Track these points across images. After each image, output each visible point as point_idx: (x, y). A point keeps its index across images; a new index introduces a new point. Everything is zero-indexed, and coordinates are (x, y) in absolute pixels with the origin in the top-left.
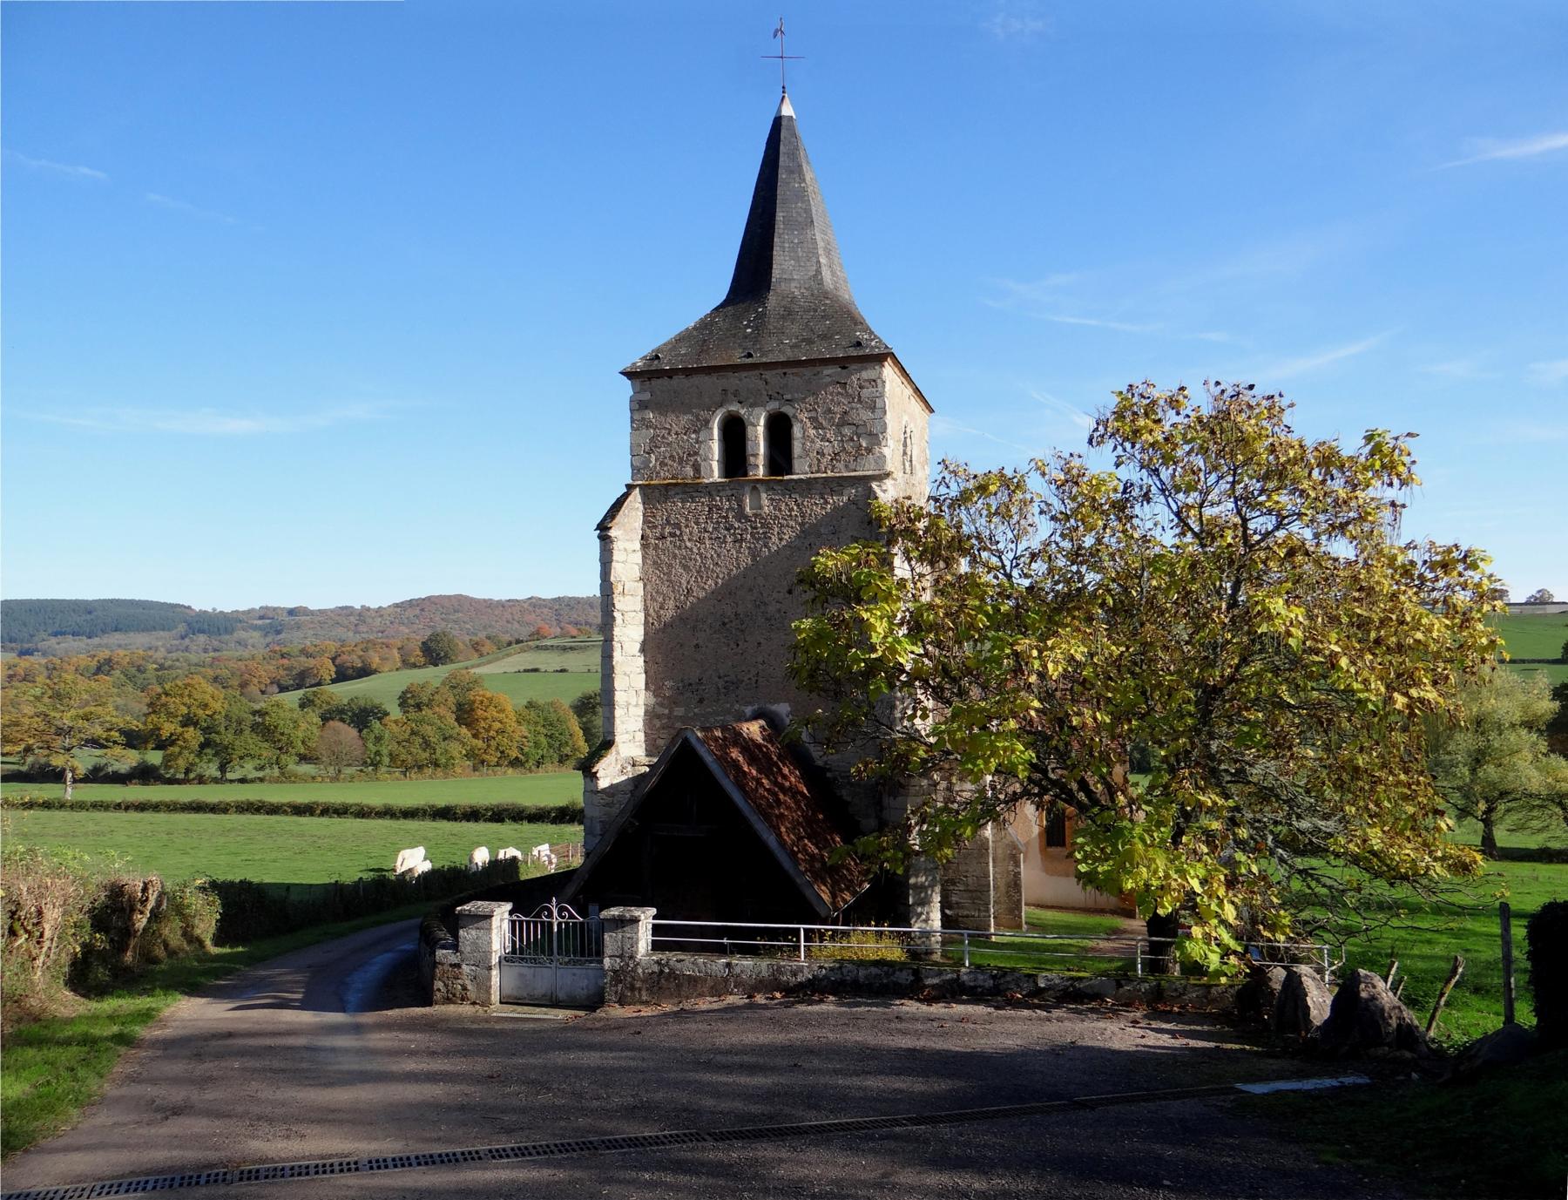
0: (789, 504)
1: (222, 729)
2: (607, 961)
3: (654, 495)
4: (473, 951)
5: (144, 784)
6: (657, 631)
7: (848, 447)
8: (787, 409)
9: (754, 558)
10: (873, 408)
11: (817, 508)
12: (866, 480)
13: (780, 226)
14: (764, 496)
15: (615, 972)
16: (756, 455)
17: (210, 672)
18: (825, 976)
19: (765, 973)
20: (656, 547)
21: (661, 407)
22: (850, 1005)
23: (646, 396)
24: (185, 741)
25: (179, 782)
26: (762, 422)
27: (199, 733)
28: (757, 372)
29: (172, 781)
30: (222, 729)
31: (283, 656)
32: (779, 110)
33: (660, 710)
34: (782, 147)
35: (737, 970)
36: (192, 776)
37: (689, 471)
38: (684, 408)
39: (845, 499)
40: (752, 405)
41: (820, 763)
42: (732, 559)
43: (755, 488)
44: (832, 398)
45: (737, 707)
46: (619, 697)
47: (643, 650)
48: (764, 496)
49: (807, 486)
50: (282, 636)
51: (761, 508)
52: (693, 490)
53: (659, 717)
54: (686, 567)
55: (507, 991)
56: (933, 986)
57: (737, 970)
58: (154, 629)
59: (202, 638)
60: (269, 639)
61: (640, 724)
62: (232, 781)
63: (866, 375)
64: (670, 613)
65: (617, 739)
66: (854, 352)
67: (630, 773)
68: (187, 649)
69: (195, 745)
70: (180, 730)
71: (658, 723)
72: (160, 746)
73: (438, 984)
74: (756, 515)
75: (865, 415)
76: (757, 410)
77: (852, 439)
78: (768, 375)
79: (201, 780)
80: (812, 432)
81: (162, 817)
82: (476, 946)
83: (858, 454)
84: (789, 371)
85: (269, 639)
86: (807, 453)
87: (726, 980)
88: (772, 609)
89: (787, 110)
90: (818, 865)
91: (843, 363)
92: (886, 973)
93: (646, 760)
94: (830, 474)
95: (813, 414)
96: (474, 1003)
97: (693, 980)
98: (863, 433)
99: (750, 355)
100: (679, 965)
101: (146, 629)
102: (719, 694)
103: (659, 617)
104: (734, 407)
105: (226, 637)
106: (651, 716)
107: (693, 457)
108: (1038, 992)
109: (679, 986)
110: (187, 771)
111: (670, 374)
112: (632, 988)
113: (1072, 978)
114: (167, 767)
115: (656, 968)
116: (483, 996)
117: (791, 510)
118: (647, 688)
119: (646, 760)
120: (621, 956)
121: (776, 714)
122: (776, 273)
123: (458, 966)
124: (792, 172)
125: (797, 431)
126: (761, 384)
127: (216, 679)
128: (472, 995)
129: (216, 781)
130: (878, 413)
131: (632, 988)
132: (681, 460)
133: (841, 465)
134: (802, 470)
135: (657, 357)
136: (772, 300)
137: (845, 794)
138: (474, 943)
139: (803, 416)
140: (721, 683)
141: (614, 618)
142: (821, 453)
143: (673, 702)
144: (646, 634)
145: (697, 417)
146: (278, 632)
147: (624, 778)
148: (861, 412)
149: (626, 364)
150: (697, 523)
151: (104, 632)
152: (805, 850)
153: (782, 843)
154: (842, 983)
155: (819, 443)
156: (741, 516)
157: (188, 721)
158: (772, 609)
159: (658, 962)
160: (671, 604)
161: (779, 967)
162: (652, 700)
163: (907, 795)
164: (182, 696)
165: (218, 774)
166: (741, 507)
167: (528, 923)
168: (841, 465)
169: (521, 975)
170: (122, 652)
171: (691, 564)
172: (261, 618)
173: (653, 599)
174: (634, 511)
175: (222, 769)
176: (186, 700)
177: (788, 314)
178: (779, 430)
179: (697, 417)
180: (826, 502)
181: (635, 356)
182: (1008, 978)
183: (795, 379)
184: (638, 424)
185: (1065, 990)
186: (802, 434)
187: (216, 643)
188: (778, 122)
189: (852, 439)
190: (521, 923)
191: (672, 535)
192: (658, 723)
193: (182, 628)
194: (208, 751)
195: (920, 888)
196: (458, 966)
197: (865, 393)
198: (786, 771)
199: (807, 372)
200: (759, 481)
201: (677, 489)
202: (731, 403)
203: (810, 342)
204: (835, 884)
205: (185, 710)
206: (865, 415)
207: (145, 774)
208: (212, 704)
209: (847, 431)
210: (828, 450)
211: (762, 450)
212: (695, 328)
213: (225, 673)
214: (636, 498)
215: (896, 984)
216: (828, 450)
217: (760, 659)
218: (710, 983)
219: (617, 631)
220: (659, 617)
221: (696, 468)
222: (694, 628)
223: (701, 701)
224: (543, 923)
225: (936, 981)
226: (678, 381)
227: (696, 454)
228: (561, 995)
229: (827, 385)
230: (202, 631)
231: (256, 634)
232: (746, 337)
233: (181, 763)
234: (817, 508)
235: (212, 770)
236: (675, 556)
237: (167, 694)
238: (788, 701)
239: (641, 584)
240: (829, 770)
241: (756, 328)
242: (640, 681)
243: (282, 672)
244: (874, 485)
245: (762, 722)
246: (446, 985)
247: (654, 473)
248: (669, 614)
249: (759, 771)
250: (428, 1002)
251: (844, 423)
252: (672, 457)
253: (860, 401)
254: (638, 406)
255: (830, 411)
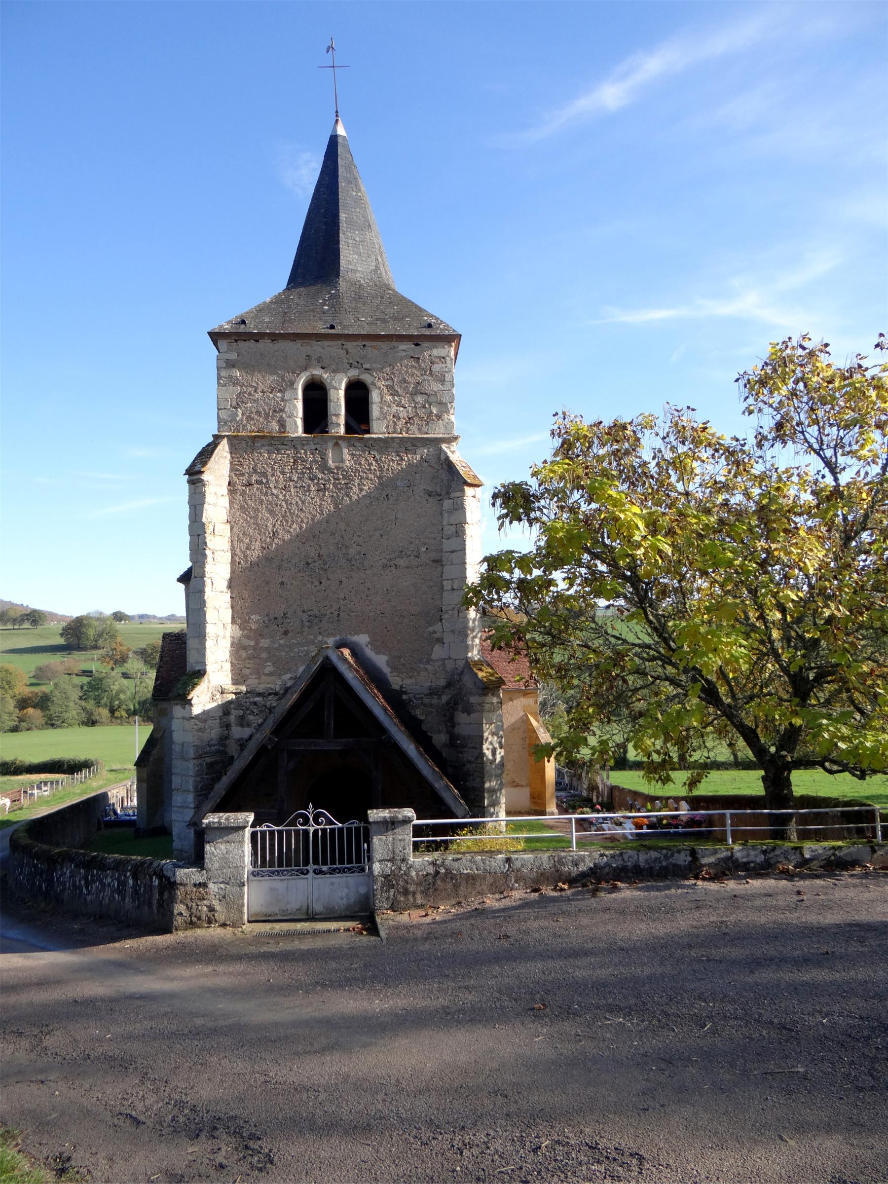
0: (368, 460)
2: (377, 867)
3: (242, 446)
4: (221, 868)
7: (421, 412)
8: (366, 378)
9: (336, 506)
10: (442, 381)
11: (394, 464)
12: (437, 442)
13: (343, 226)
14: (345, 451)
15: (386, 877)
16: (337, 415)
18: (607, 865)
19: (546, 866)
20: (243, 493)
21: (248, 367)
22: (648, 889)
23: (234, 356)
26: (343, 386)
28: (339, 342)
32: (335, 129)
33: (246, 642)
34: (339, 160)
35: (518, 865)
37: (275, 426)
38: (271, 369)
39: (418, 457)
40: (334, 371)
41: (396, 687)
42: (315, 506)
43: (337, 444)
44: (405, 369)
45: (320, 638)
46: (210, 629)
47: (230, 587)
48: (345, 451)
49: (384, 445)
51: (342, 461)
52: (278, 442)
53: (245, 648)
54: (272, 512)
55: (256, 909)
56: (710, 865)
57: (518, 865)
61: (227, 655)
63: (436, 352)
64: (257, 553)
65: (209, 668)
66: (427, 332)
67: (220, 700)
71: (244, 654)
73: (179, 908)
74: (338, 468)
75: (436, 387)
76: (339, 376)
77: (424, 407)
78: (350, 345)
80: (389, 398)
82: (225, 860)
83: (430, 419)
84: (368, 343)
86: (384, 416)
87: (506, 876)
88: (352, 551)
89: (341, 131)
91: (416, 340)
92: (666, 857)
93: (233, 688)
94: (405, 435)
95: (390, 383)
96: (224, 925)
97: (471, 879)
98: (434, 402)
99: (332, 327)
100: (456, 865)
102: (303, 626)
103: (246, 557)
104: (318, 372)
106: (237, 647)
107: (278, 412)
108: (804, 863)
109: (456, 887)
111: (257, 337)
112: (406, 892)
113: (833, 848)
115: (431, 870)
116: (234, 916)
117: (370, 465)
118: (233, 622)
119: (233, 688)
120: (392, 860)
122: (343, 263)
123: (204, 885)
124: (349, 182)
125: (375, 396)
126: (342, 353)
128: (221, 916)
130: (447, 386)
131: (406, 892)
132: (267, 416)
133: (414, 428)
134: (379, 429)
135: (243, 322)
136: (343, 285)
138: (224, 859)
139: (381, 384)
140: (305, 617)
141: (205, 556)
142: (396, 417)
143: (259, 634)
145: (283, 378)
147: (214, 704)
148: (433, 384)
149: (214, 326)
150: (283, 473)
154: (624, 869)
155: (394, 408)
156: (324, 467)
158: (352, 551)
159: (434, 863)
161: (560, 859)
162: (238, 633)
163: (482, 711)
166: (324, 459)
167: (280, 833)
168: (414, 428)
169: (272, 890)
171: (277, 509)
174: (222, 456)
177: (358, 296)
178: (358, 399)
179: (283, 378)
180: (402, 460)
181: (223, 321)
182: (777, 852)
183: (373, 350)
184: (223, 381)
185: (828, 860)
186: (379, 401)
188: (334, 141)
189: (424, 407)
190: (272, 833)
191: (259, 482)
192: (244, 654)
195: (492, 791)
196: (204, 885)
197: (436, 368)
199: (384, 346)
200: (341, 437)
201: (264, 442)
202: (315, 367)
203: (384, 321)
206: (436, 387)
209: (420, 399)
210: (403, 414)
211: (343, 412)
212: (271, 302)
214: (223, 448)
215: (675, 866)
216: (403, 414)
217: (342, 596)
218: (489, 880)
219: (208, 568)
220: (246, 557)
221: (282, 424)
222: (280, 567)
223: (286, 633)
224: (297, 832)
225: (711, 860)
226: (265, 344)
227: (282, 411)
228: (318, 907)
229: (402, 359)
232: (324, 312)
234: (394, 464)
236: (261, 502)
238: (368, 632)
239: (228, 526)
240: (405, 693)
241: (332, 306)
242: (228, 614)
244: (444, 446)
246: (189, 908)
247: (240, 426)
248: (255, 554)
250: (166, 929)
251: (416, 392)
252: (258, 413)
253: (431, 374)
254: (226, 365)
255: (405, 381)
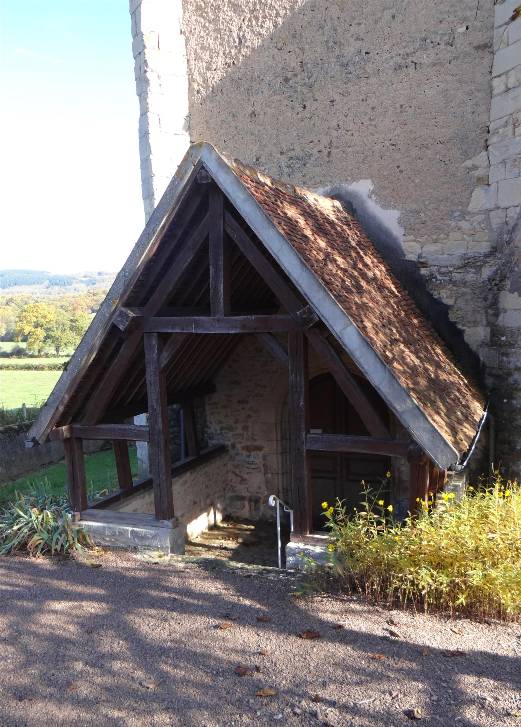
1: (55, 329)
5: (19, 358)
6: (204, 100)
17: (59, 304)
24: (37, 335)
25: (36, 357)
27: (43, 331)
29: (32, 356)
30: (55, 329)
31: (94, 295)
36: (42, 353)
41: (411, 257)
50: (95, 286)
58: (34, 283)
59: (57, 288)
60: (89, 287)
62: (62, 356)
64: (220, 74)
68: (50, 293)
69: (42, 338)
70: (33, 330)
72: (25, 340)
79: (47, 356)
81: (10, 372)
85: (89, 287)
90: (423, 382)
101: (29, 284)
103: (206, 81)
105: (68, 287)
110: (39, 351)
114: (30, 349)
121: (355, 195)
127: (62, 307)
129: (54, 356)
137: (445, 296)
140: (284, 160)
144: (191, 106)
146: (94, 284)
151: (10, 285)
152: (402, 360)
153: (369, 344)
157: (37, 325)
158: (349, 51)
160: (219, 62)
164: (33, 311)
165: (55, 353)
170: (17, 295)
172: (85, 277)
173: (197, 58)
175: (57, 349)
176: (35, 314)
187: (64, 290)
193: (47, 283)
194: (49, 340)
198: (368, 260)
204: (450, 412)
205: (35, 319)
207: (19, 353)
208: (49, 316)
213: (66, 304)
217: (334, 123)
220: (206, 81)
230: (57, 284)
231: (83, 285)
233: (36, 347)
235: (52, 350)
237: (25, 311)
238: (371, 176)
240: (424, 265)
243: (94, 303)
245: (337, 203)
248: (216, 77)
249: (329, 243)
